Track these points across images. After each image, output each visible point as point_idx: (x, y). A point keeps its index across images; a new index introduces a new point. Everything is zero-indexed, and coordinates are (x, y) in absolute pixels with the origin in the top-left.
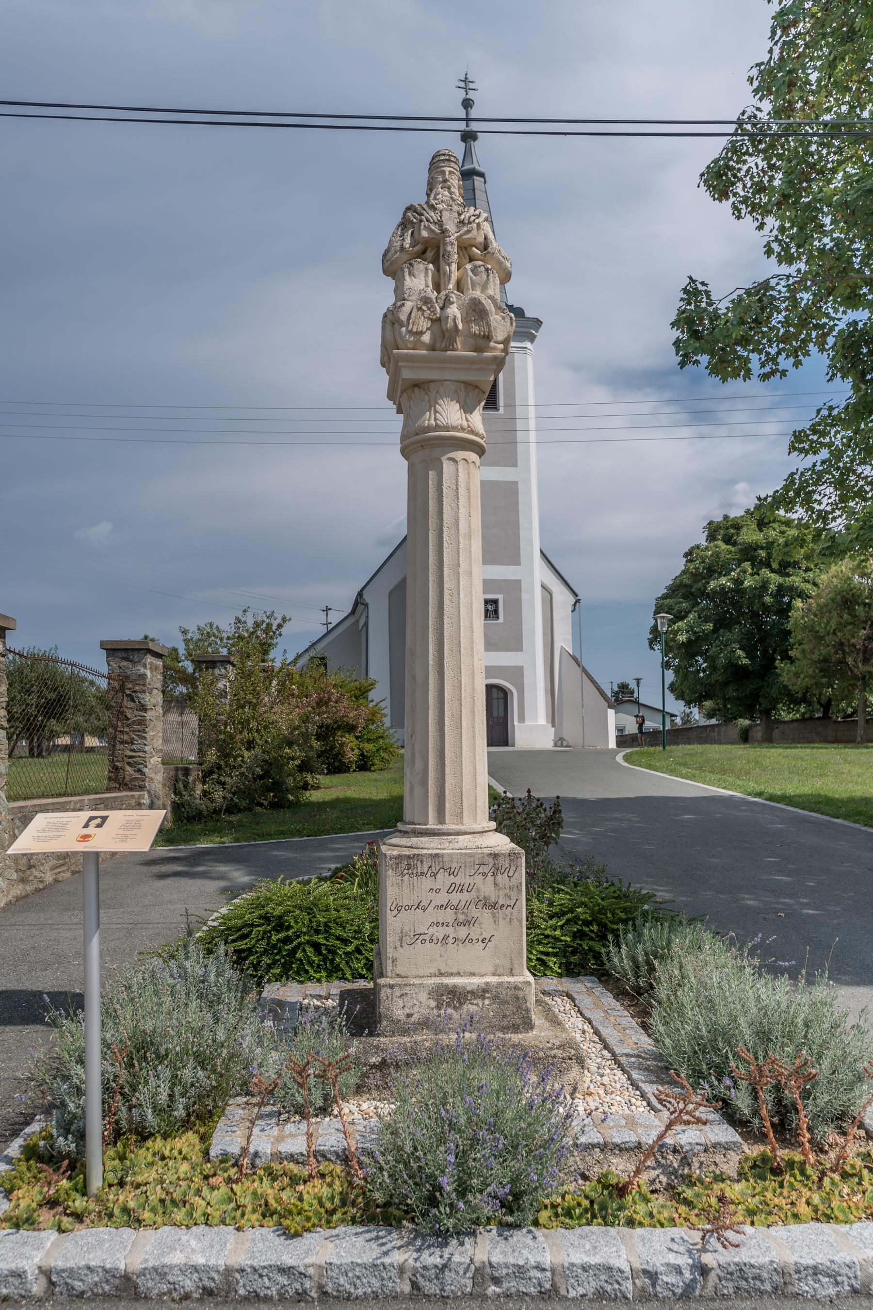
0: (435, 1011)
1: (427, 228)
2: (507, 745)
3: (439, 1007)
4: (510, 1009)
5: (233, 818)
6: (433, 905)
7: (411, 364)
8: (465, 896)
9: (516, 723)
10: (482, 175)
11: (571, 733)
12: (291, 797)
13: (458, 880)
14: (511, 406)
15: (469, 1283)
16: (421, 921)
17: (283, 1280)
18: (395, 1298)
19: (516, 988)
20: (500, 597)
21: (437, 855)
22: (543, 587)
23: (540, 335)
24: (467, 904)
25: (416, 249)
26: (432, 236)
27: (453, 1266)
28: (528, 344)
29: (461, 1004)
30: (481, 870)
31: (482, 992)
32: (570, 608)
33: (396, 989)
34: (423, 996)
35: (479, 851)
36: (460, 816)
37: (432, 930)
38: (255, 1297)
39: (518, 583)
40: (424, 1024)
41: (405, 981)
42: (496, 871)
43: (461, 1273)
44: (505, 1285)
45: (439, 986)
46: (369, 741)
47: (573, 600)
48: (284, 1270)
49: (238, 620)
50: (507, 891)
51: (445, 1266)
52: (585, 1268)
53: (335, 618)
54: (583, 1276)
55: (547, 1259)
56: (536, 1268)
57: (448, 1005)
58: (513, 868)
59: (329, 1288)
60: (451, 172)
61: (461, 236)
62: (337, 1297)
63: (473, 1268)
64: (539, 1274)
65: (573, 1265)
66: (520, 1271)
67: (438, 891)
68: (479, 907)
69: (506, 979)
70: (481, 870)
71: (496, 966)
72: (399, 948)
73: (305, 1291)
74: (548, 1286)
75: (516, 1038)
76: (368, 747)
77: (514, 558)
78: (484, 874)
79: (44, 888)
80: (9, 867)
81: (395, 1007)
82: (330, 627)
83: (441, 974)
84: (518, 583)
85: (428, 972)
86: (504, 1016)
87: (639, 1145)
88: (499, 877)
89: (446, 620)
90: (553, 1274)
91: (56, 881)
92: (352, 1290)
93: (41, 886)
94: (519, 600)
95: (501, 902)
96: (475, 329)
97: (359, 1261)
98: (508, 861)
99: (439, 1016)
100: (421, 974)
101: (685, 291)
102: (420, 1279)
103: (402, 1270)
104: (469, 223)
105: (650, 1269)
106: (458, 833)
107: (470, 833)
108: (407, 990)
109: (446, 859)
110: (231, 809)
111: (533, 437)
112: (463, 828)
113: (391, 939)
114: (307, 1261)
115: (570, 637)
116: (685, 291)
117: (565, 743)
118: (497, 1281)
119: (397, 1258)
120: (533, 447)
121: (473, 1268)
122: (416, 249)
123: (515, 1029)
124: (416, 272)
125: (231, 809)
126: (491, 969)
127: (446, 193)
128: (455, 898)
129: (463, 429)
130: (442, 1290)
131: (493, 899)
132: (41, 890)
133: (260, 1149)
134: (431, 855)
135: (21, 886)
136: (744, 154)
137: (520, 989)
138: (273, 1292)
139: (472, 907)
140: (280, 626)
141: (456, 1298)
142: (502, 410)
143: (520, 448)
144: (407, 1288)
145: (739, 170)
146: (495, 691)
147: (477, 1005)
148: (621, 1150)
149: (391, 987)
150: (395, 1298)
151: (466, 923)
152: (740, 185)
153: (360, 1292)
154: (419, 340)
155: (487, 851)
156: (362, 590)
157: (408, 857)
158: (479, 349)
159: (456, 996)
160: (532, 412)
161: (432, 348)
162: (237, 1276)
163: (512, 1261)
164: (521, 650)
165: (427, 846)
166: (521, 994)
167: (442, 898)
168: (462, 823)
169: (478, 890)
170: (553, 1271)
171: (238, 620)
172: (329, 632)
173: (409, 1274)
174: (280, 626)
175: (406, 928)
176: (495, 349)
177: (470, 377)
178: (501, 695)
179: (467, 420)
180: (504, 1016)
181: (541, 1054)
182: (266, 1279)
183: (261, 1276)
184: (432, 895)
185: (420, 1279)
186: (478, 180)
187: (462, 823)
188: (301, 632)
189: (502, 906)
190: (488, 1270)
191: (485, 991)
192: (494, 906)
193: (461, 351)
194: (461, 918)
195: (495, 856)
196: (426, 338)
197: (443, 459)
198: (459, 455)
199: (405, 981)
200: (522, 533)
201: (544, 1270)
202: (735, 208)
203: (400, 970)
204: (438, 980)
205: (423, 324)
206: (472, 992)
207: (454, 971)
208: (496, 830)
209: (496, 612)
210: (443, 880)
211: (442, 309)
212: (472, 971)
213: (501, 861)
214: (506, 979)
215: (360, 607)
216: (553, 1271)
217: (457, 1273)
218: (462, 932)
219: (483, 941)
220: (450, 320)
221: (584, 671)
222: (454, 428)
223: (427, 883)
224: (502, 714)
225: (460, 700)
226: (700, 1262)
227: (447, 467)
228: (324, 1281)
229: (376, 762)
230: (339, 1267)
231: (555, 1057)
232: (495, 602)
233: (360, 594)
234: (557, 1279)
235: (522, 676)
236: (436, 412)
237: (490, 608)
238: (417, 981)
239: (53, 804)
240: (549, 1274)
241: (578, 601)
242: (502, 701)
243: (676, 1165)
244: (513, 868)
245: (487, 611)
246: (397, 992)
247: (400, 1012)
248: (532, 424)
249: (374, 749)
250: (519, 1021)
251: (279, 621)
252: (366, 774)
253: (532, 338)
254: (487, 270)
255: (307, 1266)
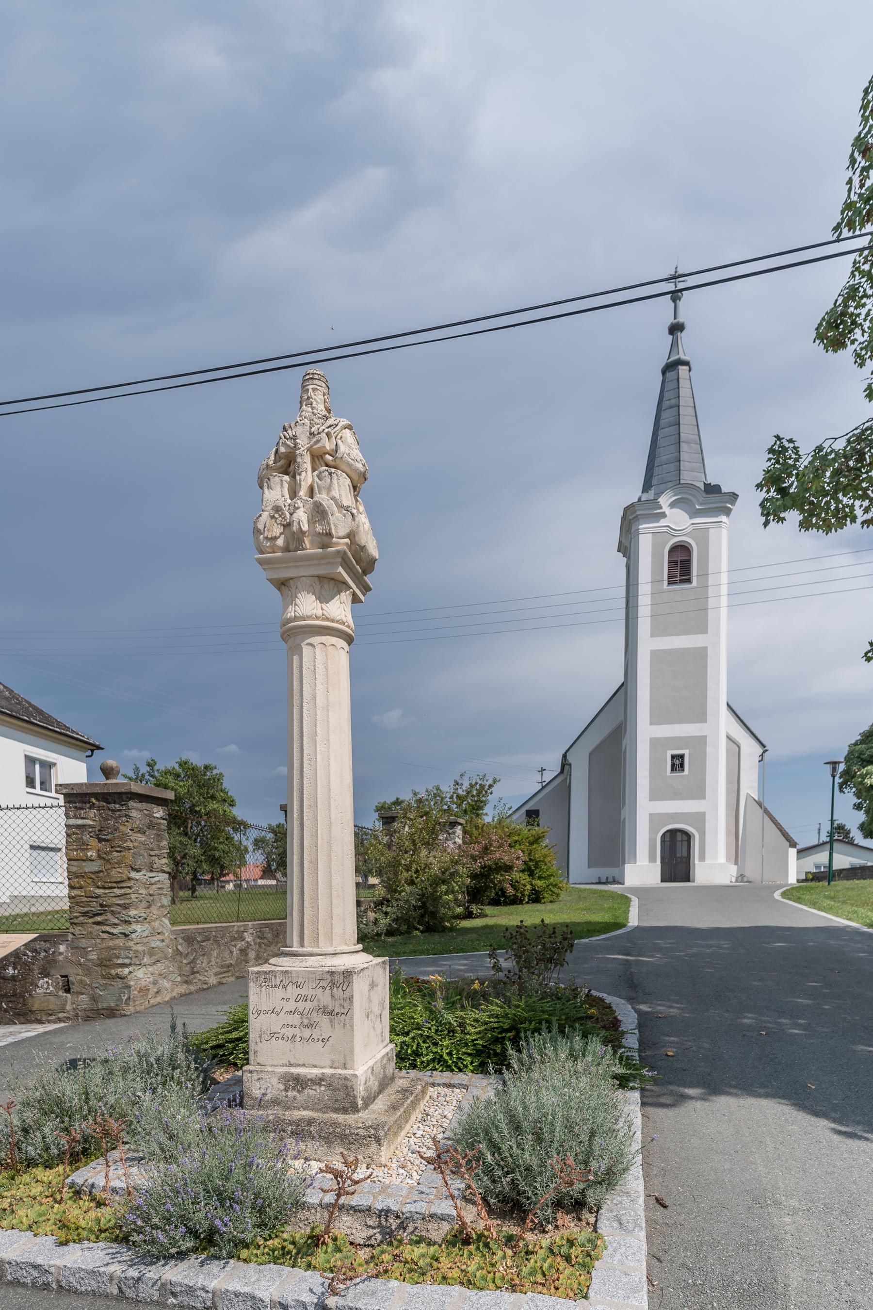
0: (283, 1093)
1: (284, 444)
2: (689, 881)
3: (286, 1090)
4: (341, 1095)
5: (390, 939)
6: (284, 1011)
7: (271, 566)
8: (309, 1005)
9: (697, 862)
10: (687, 363)
11: (752, 871)
12: (448, 924)
13: (303, 992)
14: (704, 575)
15: (157, 1294)
16: (275, 1023)
17: (35, 1273)
18: (107, 1296)
19: (346, 1079)
20: (686, 752)
21: (286, 972)
22: (729, 738)
23: (736, 509)
24: (311, 1011)
25: (279, 464)
26: (289, 450)
27: (144, 1279)
28: (724, 518)
29: (303, 1088)
30: (321, 985)
31: (319, 1081)
32: (758, 759)
33: (254, 1074)
34: (274, 1081)
35: (320, 969)
36: (316, 940)
37: (284, 1030)
38: (16, 1283)
39: (704, 738)
40: (276, 1102)
41: (263, 1068)
42: (333, 984)
43: (150, 1285)
44: (180, 1299)
45: (286, 1074)
46: (540, 878)
47: (761, 751)
48: (36, 1267)
49: (457, 783)
50: (342, 1002)
51: (139, 1279)
52: (237, 1295)
53: (548, 777)
54: (235, 1300)
55: (212, 1285)
56: (203, 1289)
57: (293, 1089)
58: (346, 983)
59: (63, 1284)
60: (314, 390)
61: (312, 446)
62: (68, 1290)
63: (159, 1283)
64: (204, 1295)
65: (227, 1291)
66: (190, 1290)
67: (288, 1000)
68: (320, 1013)
69: (340, 1071)
70: (321, 985)
71: (333, 1061)
72: (259, 1043)
73: (48, 1283)
74: (209, 1304)
75: (341, 1118)
76: (539, 883)
77: (700, 715)
78: (323, 988)
79: (208, 988)
80: (173, 972)
81: (255, 1089)
82: (544, 784)
83: (291, 1065)
84: (704, 738)
85: (281, 1062)
86: (336, 1101)
87: (369, 1209)
88: (335, 990)
89: (305, 781)
90: (213, 1296)
91: (220, 983)
92: (78, 1287)
93: (205, 987)
94: (704, 754)
95: (336, 1010)
96: (319, 528)
97: (83, 1267)
98: (342, 977)
99: (286, 1097)
100: (276, 1063)
101: (771, 451)
102: (123, 1286)
103: (111, 1278)
104: (319, 433)
105: (283, 1302)
106: (311, 955)
107: (322, 955)
108: (262, 1075)
109: (294, 975)
110: (390, 933)
111: (724, 601)
112: (316, 950)
113: (253, 1036)
114: (52, 1263)
115: (756, 785)
116: (771, 451)
117: (745, 879)
118: (174, 1295)
119: (115, 1269)
120: (724, 612)
121: (159, 1283)
122: (279, 464)
123: (345, 1111)
124: (273, 485)
125: (390, 933)
126: (329, 1063)
127: (310, 409)
128: (301, 1005)
129: (317, 618)
130: (137, 1296)
131: (330, 1008)
132: (204, 989)
133: (97, 1183)
134: (282, 972)
135: (185, 986)
136: (862, 298)
137: (348, 1080)
138: (28, 1280)
139: (314, 1014)
140: (490, 786)
141: (146, 1303)
142: (694, 580)
143: (711, 614)
144: (115, 1291)
145: (859, 315)
146: (679, 834)
147: (315, 1090)
148: (355, 1211)
149: (251, 1072)
150: (107, 1296)
151: (309, 1026)
152: (858, 331)
153: (83, 1289)
154: (274, 544)
155: (326, 969)
156: (566, 753)
157: (265, 973)
158: (324, 546)
159: (299, 1083)
160: (724, 578)
161: (286, 549)
162: (7, 1266)
163: (186, 1282)
164: (704, 798)
165: (284, 964)
166: (349, 1084)
167: (291, 1006)
168: (318, 946)
169: (319, 1000)
170: (214, 1293)
171: (457, 783)
172: (543, 788)
173: (116, 1281)
174: (490, 786)
175: (264, 1028)
176: (338, 544)
177: (321, 571)
178: (685, 838)
179: (322, 609)
180: (336, 1101)
181: (347, 1132)
182: (24, 1271)
183: (21, 1269)
184: (284, 1003)
185: (123, 1286)
186: (683, 369)
187: (318, 946)
188: (512, 791)
189: (338, 1013)
190: (169, 1286)
191: (321, 1080)
192: (331, 1013)
193: (310, 548)
194: (306, 1022)
195: (332, 973)
196: (280, 542)
197: (303, 644)
198: (316, 640)
199: (263, 1068)
200: (709, 694)
201: (207, 1292)
202: (858, 356)
203: (260, 1060)
204: (286, 1069)
205: (277, 530)
206: (311, 1080)
207: (301, 1063)
208: (362, 951)
209: (682, 765)
210: (292, 992)
211: (291, 514)
212: (314, 1063)
213: (336, 977)
214: (340, 1071)
215: (567, 767)
216: (214, 1293)
217: (147, 1285)
218: (307, 1033)
219: (323, 1040)
220: (295, 524)
221: (766, 812)
222: (309, 617)
223: (279, 993)
224: (685, 854)
225: (317, 846)
226: (323, 1302)
227: (306, 651)
228: (61, 1278)
229: (545, 895)
230: (70, 1269)
231: (357, 1134)
232: (682, 757)
233: (565, 756)
234: (216, 1300)
235: (704, 821)
236: (296, 605)
237: (677, 762)
238: (270, 1069)
239: (216, 927)
240: (210, 1295)
241: (764, 752)
242: (685, 844)
243: (393, 1228)
244: (346, 983)
245: (673, 765)
246: (255, 1076)
247: (257, 1092)
248: (724, 590)
249: (545, 885)
250: (348, 1105)
251: (490, 782)
252: (538, 906)
253: (728, 512)
254: (330, 474)
255: (50, 1266)
